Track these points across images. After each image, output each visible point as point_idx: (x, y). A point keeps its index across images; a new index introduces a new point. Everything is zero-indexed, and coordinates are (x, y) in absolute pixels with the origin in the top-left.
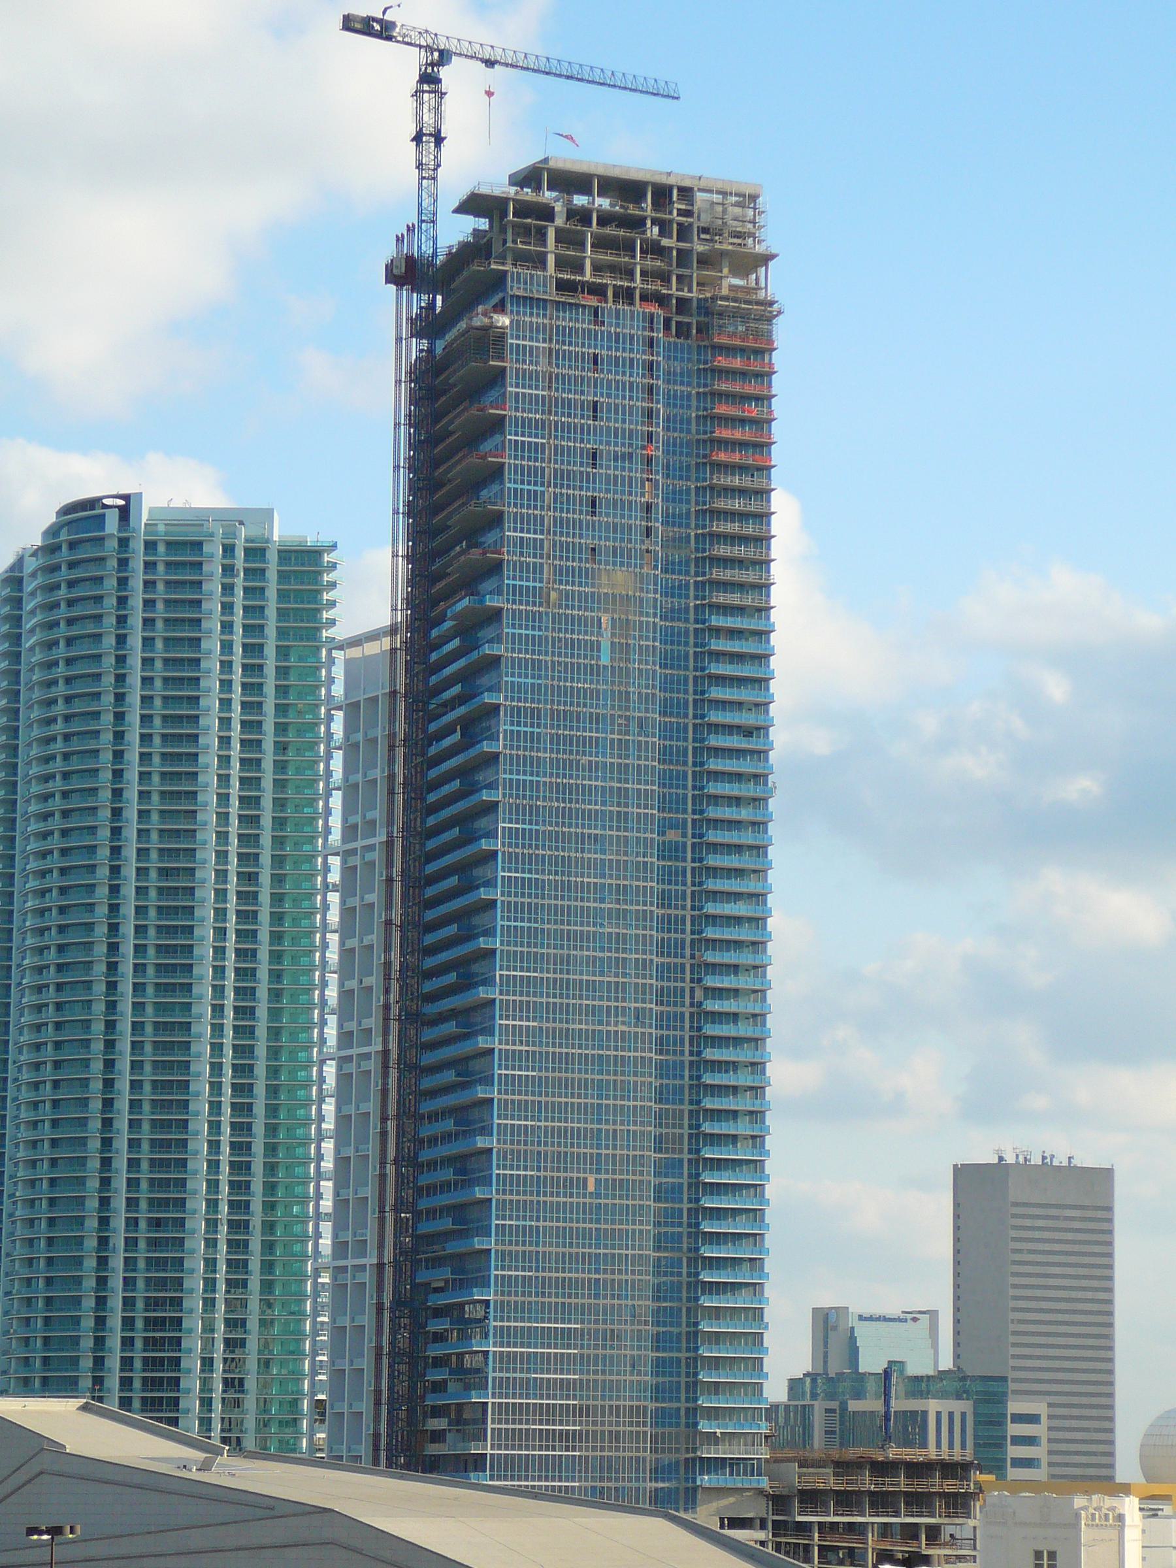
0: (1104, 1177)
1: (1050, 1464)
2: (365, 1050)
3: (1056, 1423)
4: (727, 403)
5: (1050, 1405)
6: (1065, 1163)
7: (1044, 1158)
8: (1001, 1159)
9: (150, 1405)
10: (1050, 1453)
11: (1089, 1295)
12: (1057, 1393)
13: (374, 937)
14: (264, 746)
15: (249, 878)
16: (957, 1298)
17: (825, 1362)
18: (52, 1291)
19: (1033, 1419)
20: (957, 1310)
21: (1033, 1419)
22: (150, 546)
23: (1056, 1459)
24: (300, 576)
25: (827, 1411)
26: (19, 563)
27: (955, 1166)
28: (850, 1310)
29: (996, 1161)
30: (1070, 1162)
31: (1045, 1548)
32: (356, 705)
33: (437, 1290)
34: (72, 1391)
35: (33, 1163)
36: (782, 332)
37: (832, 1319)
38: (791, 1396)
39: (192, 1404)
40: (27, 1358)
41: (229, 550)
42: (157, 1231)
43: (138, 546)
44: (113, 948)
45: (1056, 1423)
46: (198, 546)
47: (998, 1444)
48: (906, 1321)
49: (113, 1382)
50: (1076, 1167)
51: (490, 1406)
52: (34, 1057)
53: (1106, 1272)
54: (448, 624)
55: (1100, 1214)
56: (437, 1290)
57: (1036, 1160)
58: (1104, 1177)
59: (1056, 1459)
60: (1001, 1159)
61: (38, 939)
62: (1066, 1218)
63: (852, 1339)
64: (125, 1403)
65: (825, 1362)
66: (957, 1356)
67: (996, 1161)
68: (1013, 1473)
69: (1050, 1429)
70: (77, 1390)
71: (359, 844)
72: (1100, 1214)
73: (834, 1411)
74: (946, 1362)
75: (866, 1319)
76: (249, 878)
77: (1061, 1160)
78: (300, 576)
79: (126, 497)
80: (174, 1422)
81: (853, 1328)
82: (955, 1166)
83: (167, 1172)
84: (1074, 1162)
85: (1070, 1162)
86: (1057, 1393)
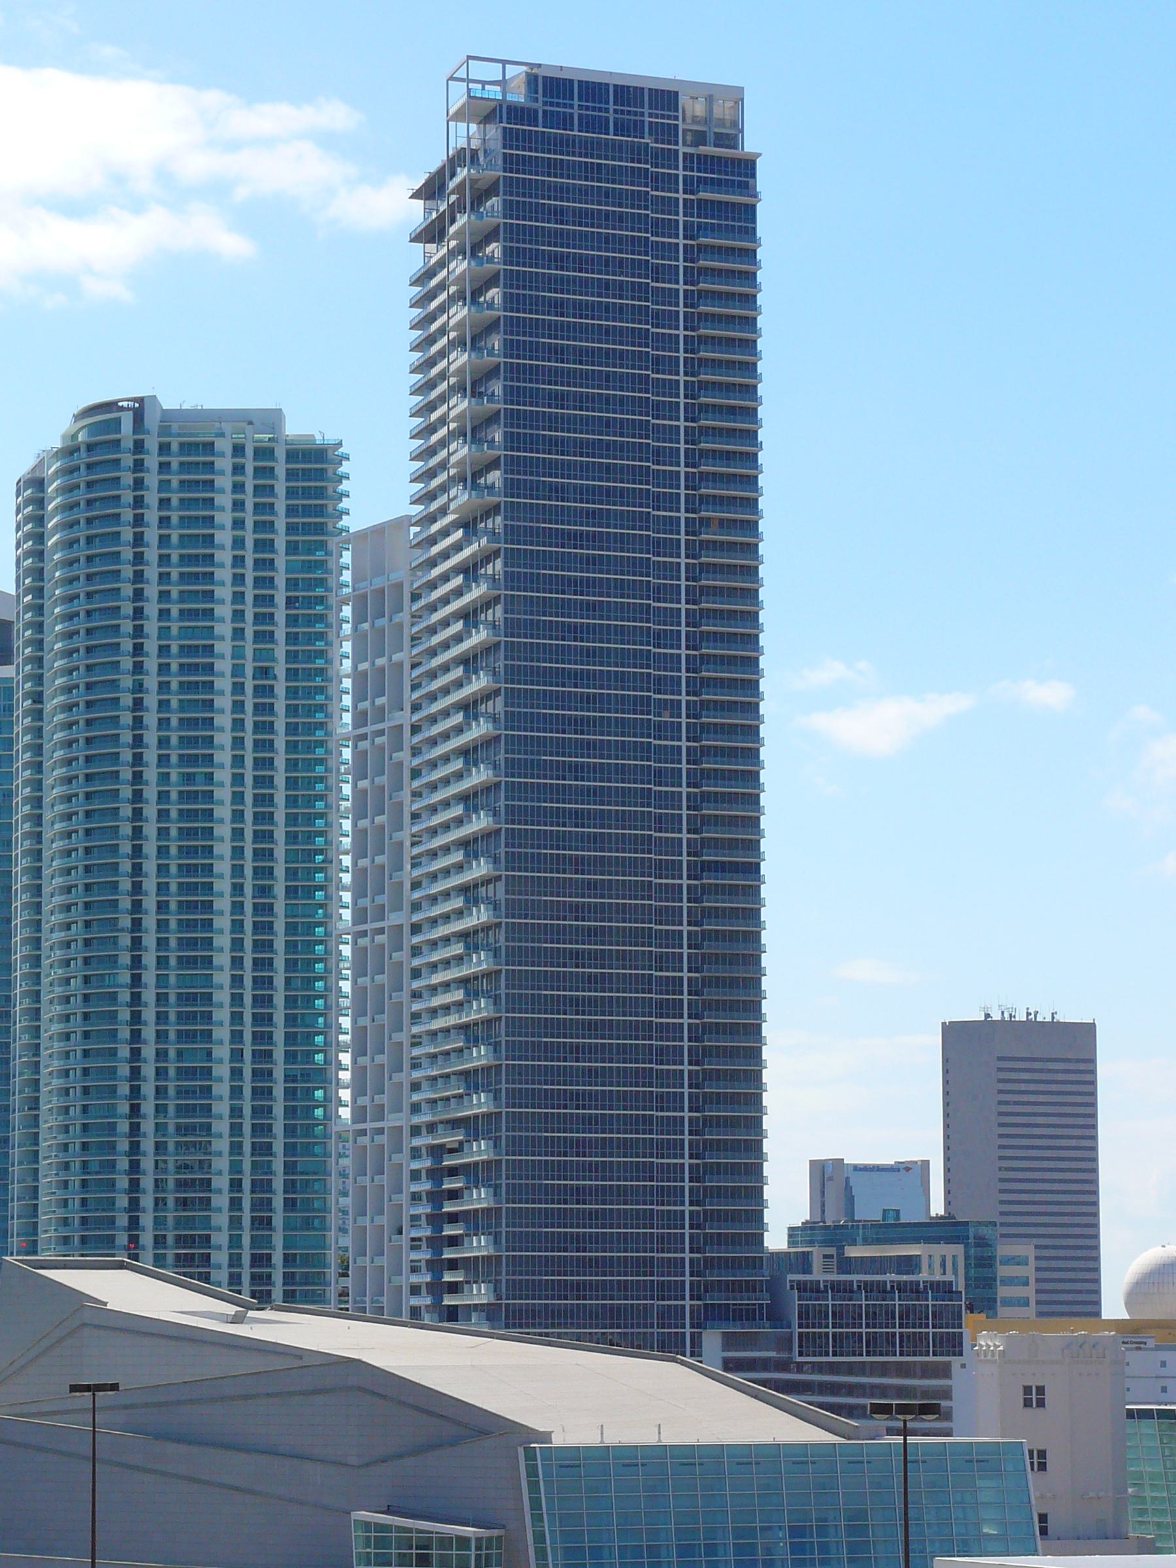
0: (1087, 1031)
1: (1038, 1303)
2: (380, 726)
3: (1044, 1264)
4: (709, 370)
5: (1037, 1247)
6: (1049, 1019)
7: (1028, 1014)
8: (987, 1015)
9: (183, 1261)
10: (1037, 1291)
11: (1073, 1143)
12: (1044, 1236)
13: (385, 778)
14: (275, 1075)
15: (264, 891)
16: (947, 1148)
17: (823, 1211)
18: (91, 896)
19: (1021, 1261)
20: (947, 1159)
21: (1021, 1261)
22: (164, 448)
23: (1044, 1297)
24: (308, 475)
25: (825, 1256)
26: (40, 465)
27: (944, 1024)
28: (845, 1162)
29: (983, 1018)
30: (1053, 1018)
31: (1034, 1383)
32: (364, 596)
33: (451, 1151)
34: (109, 1248)
35: (67, 963)
36: (764, 180)
37: (829, 1171)
38: (791, 1243)
39: (221, 1257)
40: (66, 1218)
41: (238, 450)
42: (185, 1210)
43: (152, 444)
44: (137, 924)
45: (1044, 1264)
46: (209, 447)
47: (988, 1283)
48: (899, 1170)
49: (147, 1239)
50: (1058, 1022)
51: (504, 1210)
52: (62, 1139)
53: (1089, 1121)
54: (451, 518)
55: (1082, 1066)
56: (451, 1151)
57: (1021, 1017)
58: (1087, 1031)
59: (1044, 1297)
60: (987, 1015)
61: (67, 750)
62: (1050, 1071)
63: (848, 1188)
64: (159, 1260)
65: (823, 1211)
66: (948, 1203)
67: (983, 1018)
68: (1002, 1311)
69: (1037, 1269)
70: (113, 1248)
71: (369, 1126)
72: (1082, 1066)
73: (832, 1256)
74: (937, 1207)
75: (861, 1170)
76: (264, 891)
77: (1044, 1016)
78: (308, 475)
79: (141, 400)
80: (206, 1278)
81: (847, 1179)
82: (944, 1024)
83: (193, 1005)
84: (1058, 1018)
85: (1053, 1018)
86: (1044, 1236)
